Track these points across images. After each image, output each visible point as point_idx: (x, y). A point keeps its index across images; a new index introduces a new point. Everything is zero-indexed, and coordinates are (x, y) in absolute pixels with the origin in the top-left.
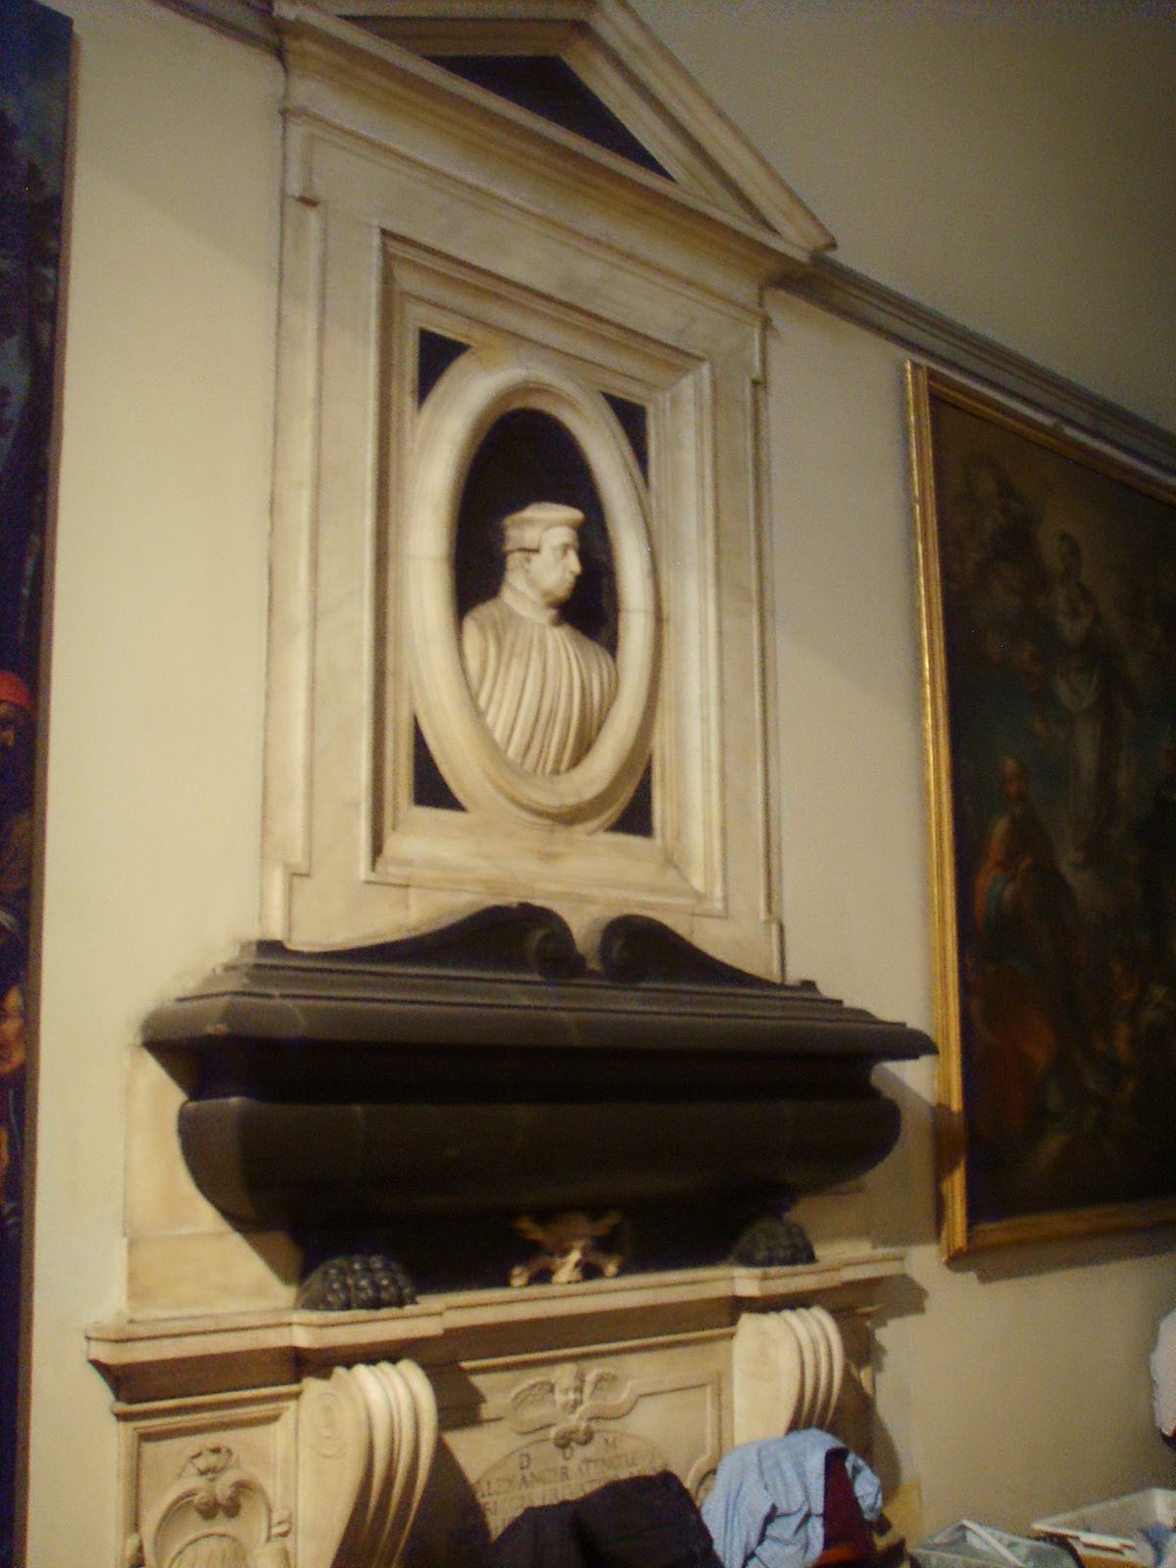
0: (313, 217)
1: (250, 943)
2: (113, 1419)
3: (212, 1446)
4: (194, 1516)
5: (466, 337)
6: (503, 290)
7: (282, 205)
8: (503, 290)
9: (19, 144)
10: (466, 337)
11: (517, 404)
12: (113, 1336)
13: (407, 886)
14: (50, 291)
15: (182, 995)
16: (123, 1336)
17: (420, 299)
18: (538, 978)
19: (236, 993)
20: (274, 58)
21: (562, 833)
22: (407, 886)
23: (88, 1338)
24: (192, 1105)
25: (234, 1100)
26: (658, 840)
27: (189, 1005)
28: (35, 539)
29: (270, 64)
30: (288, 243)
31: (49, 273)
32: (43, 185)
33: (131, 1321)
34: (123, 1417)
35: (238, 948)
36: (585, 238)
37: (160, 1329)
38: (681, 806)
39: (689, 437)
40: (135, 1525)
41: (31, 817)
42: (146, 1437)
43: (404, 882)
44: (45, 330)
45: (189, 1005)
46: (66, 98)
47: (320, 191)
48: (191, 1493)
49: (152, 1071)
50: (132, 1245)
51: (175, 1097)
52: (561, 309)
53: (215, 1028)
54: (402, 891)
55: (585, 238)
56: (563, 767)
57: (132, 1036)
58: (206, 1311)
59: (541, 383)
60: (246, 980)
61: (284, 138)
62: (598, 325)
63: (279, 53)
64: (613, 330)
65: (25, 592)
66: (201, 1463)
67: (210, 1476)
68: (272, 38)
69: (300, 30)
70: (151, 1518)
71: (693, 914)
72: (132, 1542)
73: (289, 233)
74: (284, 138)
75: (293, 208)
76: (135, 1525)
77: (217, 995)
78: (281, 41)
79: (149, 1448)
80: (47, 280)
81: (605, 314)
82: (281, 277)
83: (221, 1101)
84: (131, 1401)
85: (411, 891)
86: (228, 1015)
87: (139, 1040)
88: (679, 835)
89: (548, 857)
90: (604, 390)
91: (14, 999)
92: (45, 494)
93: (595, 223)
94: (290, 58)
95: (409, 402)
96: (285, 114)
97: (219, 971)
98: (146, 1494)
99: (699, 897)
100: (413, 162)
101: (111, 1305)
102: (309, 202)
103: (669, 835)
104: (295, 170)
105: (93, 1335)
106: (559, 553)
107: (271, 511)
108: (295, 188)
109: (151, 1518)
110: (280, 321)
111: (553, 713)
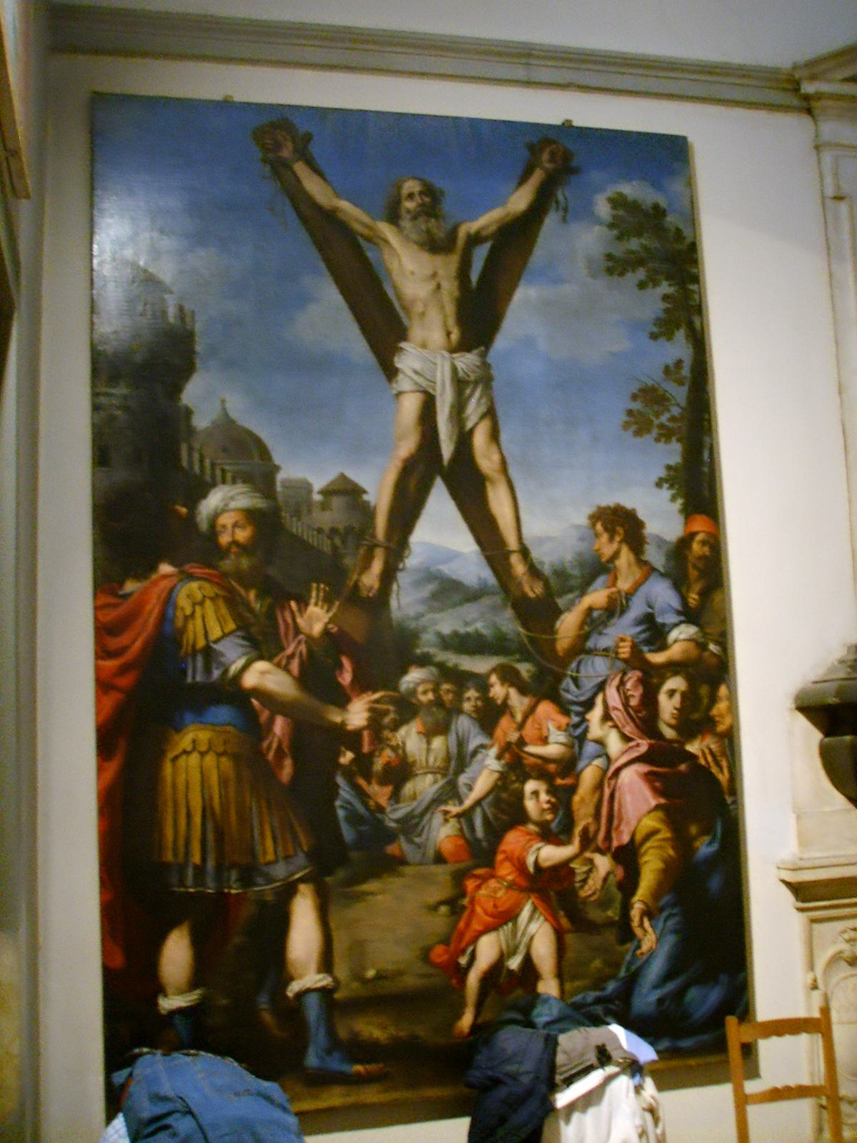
0: (843, 208)
1: (852, 646)
2: (796, 911)
3: (852, 927)
4: (843, 964)
7: (824, 205)
9: (668, 219)
12: (792, 868)
14: (696, 296)
15: (816, 680)
16: (795, 867)
19: (843, 679)
20: (806, 115)
23: (778, 868)
24: (827, 740)
25: (848, 738)
27: (819, 686)
28: (707, 439)
29: (805, 120)
30: (830, 227)
31: (693, 287)
32: (685, 238)
33: (801, 859)
34: (801, 910)
35: (846, 648)
36: (396, 293)
37: (817, 863)
40: (811, 967)
41: (723, 592)
42: (814, 921)
45: (819, 686)
46: (690, 184)
47: (846, 188)
48: (841, 952)
49: (802, 722)
50: (798, 818)
51: (816, 736)
53: (832, 700)
55: (396, 293)
57: (790, 703)
58: (842, 853)
60: (849, 670)
61: (819, 162)
63: (809, 111)
66: (846, 936)
67: (852, 943)
68: (805, 104)
69: (819, 96)
70: (821, 963)
72: (810, 976)
74: (819, 162)
75: (829, 203)
76: (811, 967)
77: (832, 680)
78: (809, 104)
79: (816, 926)
80: (694, 292)
82: (829, 249)
83: (840, 738)
84: (803, 901)
86: (838, 693)
87: (793, 706)
91: (723, 690)
92: (709, 413)
94: (816, 112)
96: (817, 148)
97: (836, 663)
98: (817, 952)
101: (789, 849)
102: (839, 198)
104: (829, 180)
105: (780, 866)
107: (840, 393)
108: (830, 192)
109: (821, 963)
110: (831, 275)
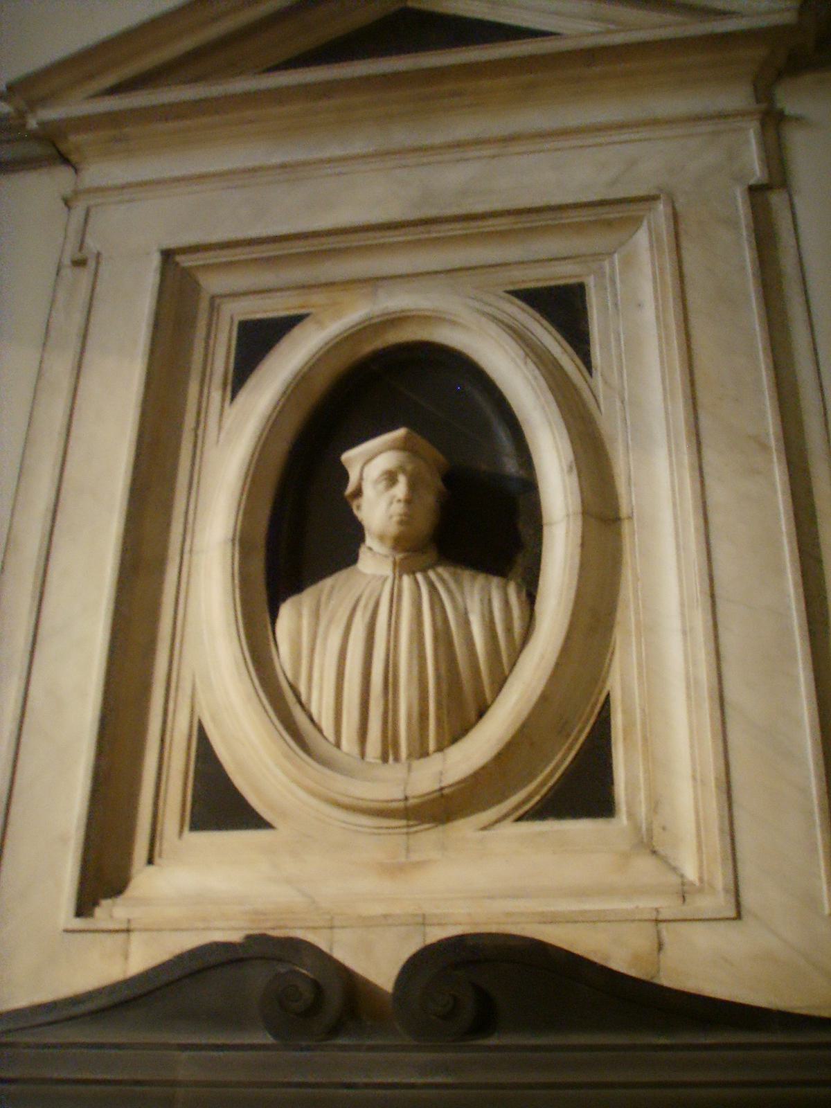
5: (303, 307)
6: (328, 243)
8: (328, 243)
10: (303, 307)
11: (368, 348)
13: (128, 931)
17: (235, 295)
18: (269, 1040)
21: (428, 838)
22: (128, 931)
26: (622, 818)
38: (655, 762)
39: (646, 290)
43: (124, 926)
52: (421, 228)
54: (123, 936)
56: (432, 745)
59: (388, 314)
62: (480, 223)
64: (503, 220)
71: (657, 921)
73: (62, 295)
75: (67, 272)
81: (480, 208)
85: (135, 937)
88: (655, 805)
89: (394, 870)
90: (511, 288)
93: (465, 127)
94: (74, 158)
95: (216, 395)
99: (684, 892)
100: (202, 177)
102: (79, 263)
103: (643, 810)
106: (382, 486)
111: (390, 683)
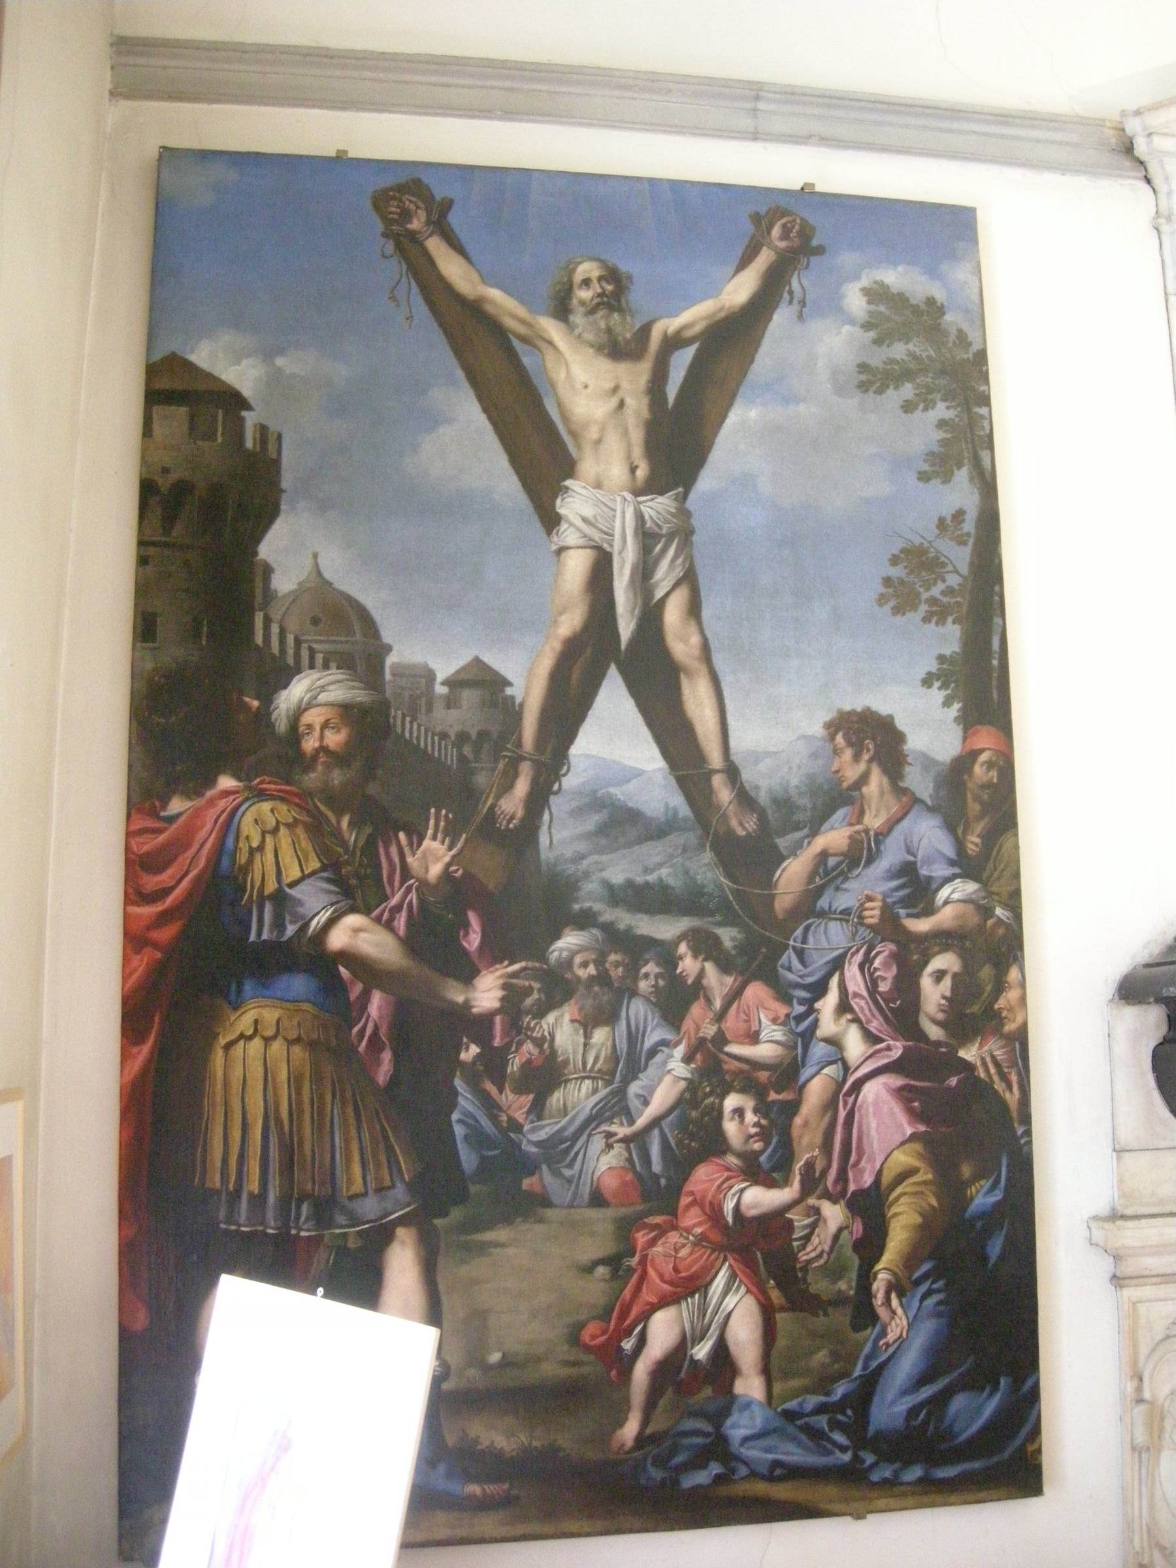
14: (986, 423)
15: (1150, 961)
31: (983, 411)
44: (985, 455)
65: (995, 662)
80: (982, 417)
